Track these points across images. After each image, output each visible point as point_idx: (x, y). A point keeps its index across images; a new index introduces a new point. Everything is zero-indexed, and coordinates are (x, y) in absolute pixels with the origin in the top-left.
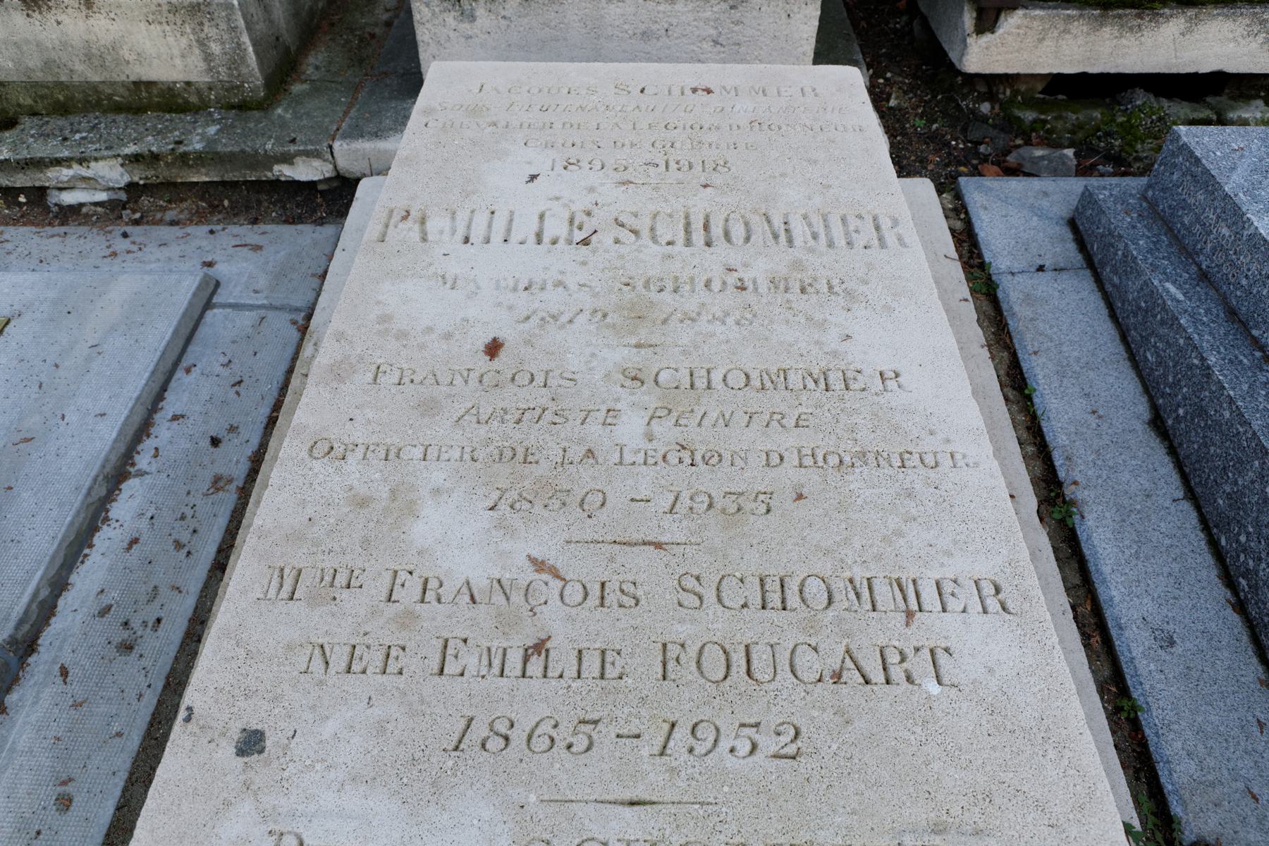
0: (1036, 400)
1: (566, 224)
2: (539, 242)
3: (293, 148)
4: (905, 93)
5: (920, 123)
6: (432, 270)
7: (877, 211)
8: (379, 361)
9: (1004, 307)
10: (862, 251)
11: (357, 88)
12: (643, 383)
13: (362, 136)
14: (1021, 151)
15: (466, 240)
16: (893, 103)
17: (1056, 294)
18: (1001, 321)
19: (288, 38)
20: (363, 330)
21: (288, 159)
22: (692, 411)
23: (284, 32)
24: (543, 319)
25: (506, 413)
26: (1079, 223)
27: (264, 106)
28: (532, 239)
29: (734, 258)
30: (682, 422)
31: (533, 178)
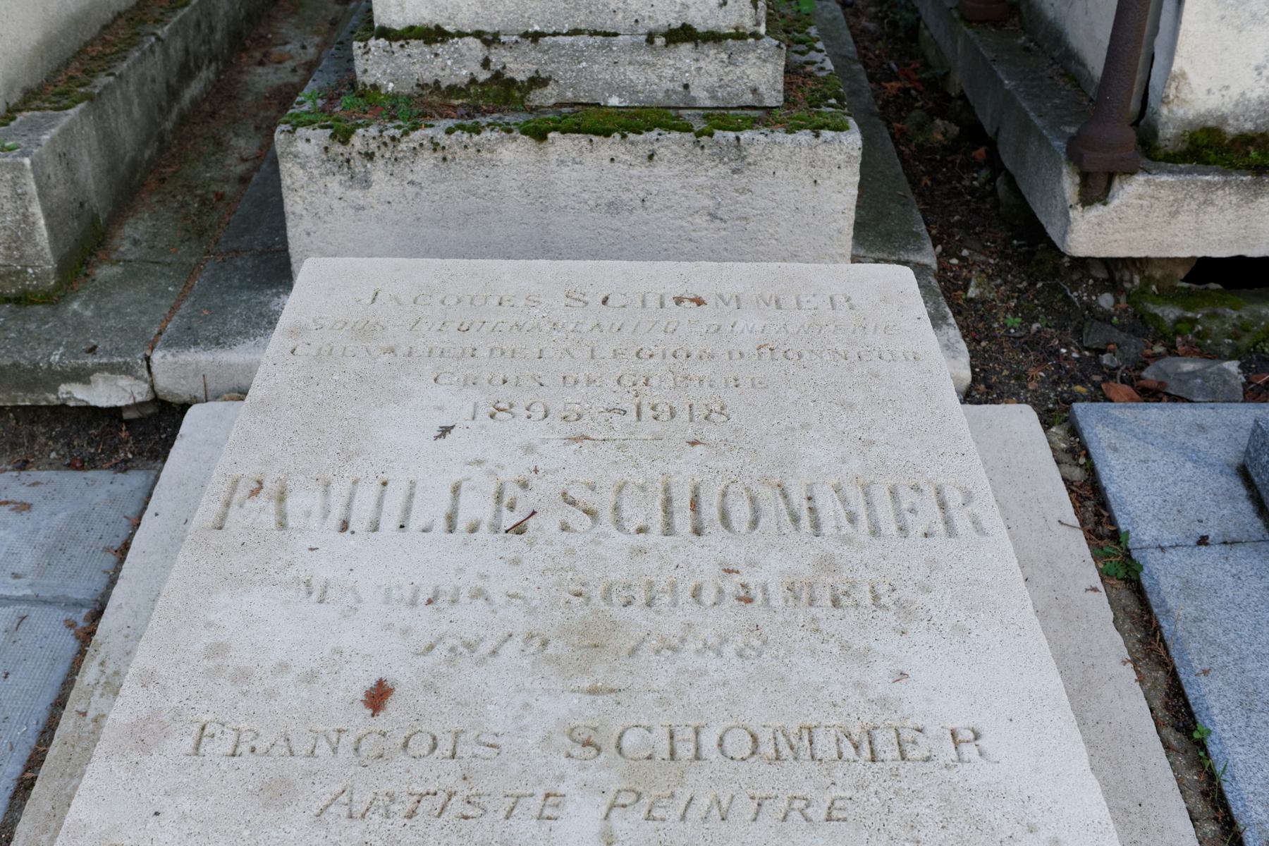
0: (1213, 749)
1: (492, 501)
2: (451, 529)
3: (91, 361)
4: (990, 278)
5: (1014, 321)
6: (292, 572)
7: (940, 480)
8: (205, 718)
9: (1153, 600)
10: (921, 541)
11: (191, 272)
12: (599, 750)
13: (196, 344)
14: (1162, 363)
15: (344, 527)
16: (972, 292)
17: (1229, 579)
18: (1150, 622)
19: (98, 205)
20: (184, 668)
21: (82, 376)
22: (672, 795)
23: (92, 195)
24: (452, 649)
25: (393, 800)
26: (1253, 473)
27: (52, 298)
28: (441, 523)
29: (735, 553)
30: (657, 813)
31: (445, 431)
